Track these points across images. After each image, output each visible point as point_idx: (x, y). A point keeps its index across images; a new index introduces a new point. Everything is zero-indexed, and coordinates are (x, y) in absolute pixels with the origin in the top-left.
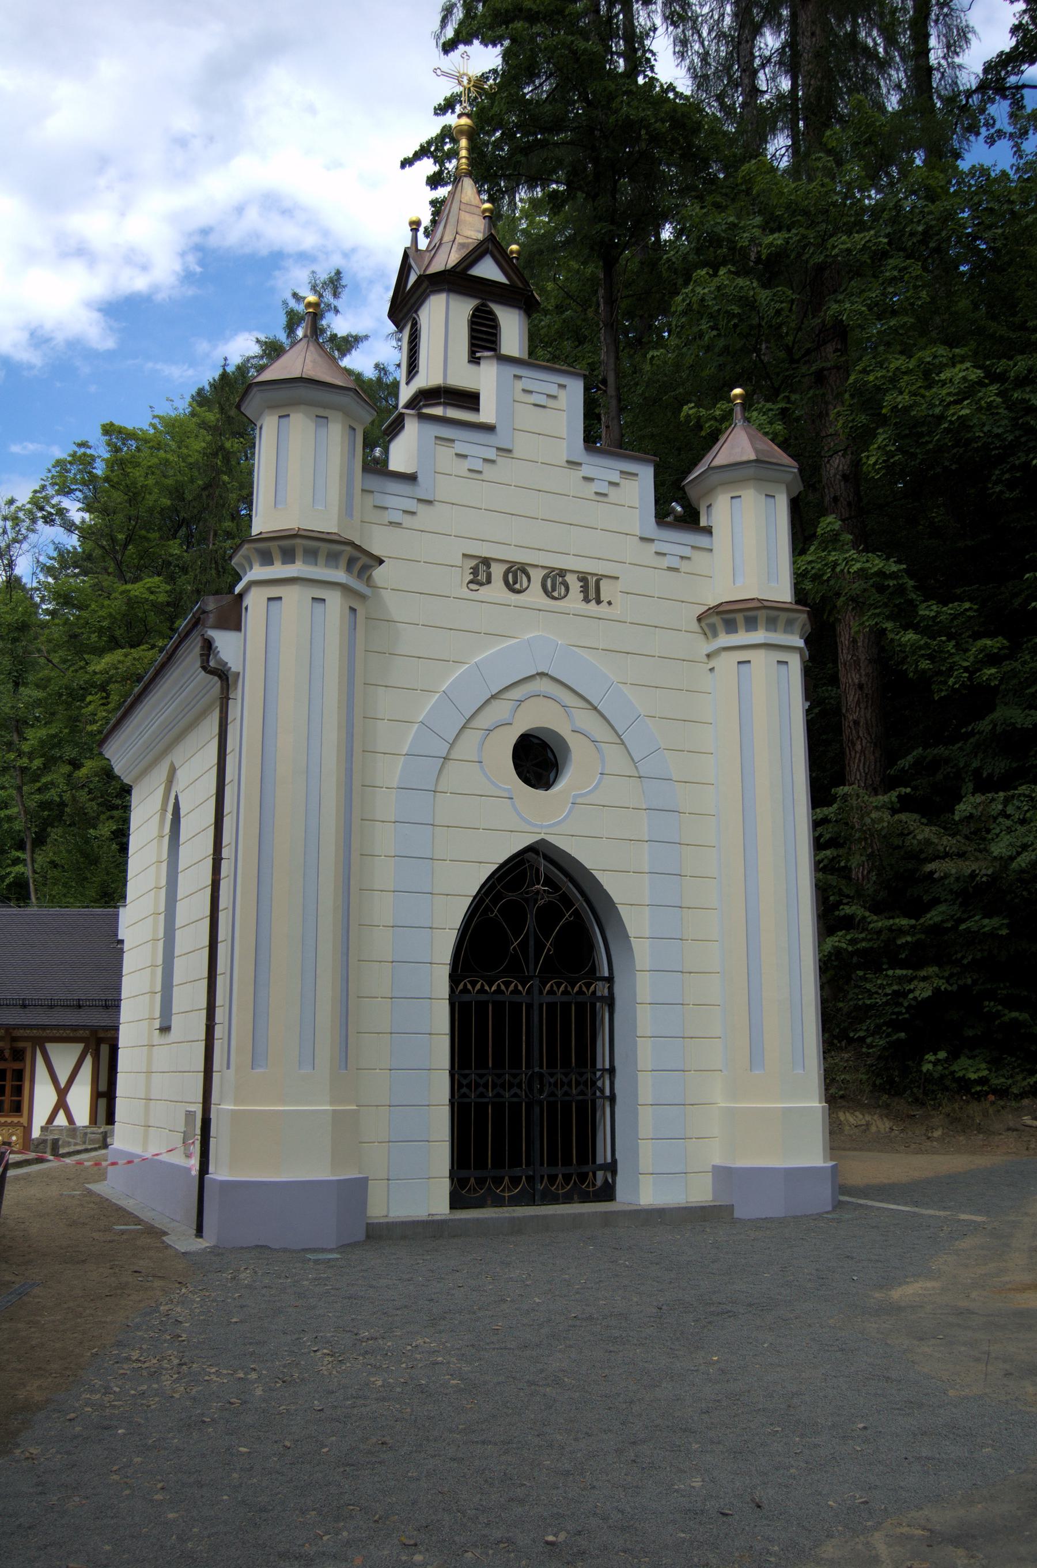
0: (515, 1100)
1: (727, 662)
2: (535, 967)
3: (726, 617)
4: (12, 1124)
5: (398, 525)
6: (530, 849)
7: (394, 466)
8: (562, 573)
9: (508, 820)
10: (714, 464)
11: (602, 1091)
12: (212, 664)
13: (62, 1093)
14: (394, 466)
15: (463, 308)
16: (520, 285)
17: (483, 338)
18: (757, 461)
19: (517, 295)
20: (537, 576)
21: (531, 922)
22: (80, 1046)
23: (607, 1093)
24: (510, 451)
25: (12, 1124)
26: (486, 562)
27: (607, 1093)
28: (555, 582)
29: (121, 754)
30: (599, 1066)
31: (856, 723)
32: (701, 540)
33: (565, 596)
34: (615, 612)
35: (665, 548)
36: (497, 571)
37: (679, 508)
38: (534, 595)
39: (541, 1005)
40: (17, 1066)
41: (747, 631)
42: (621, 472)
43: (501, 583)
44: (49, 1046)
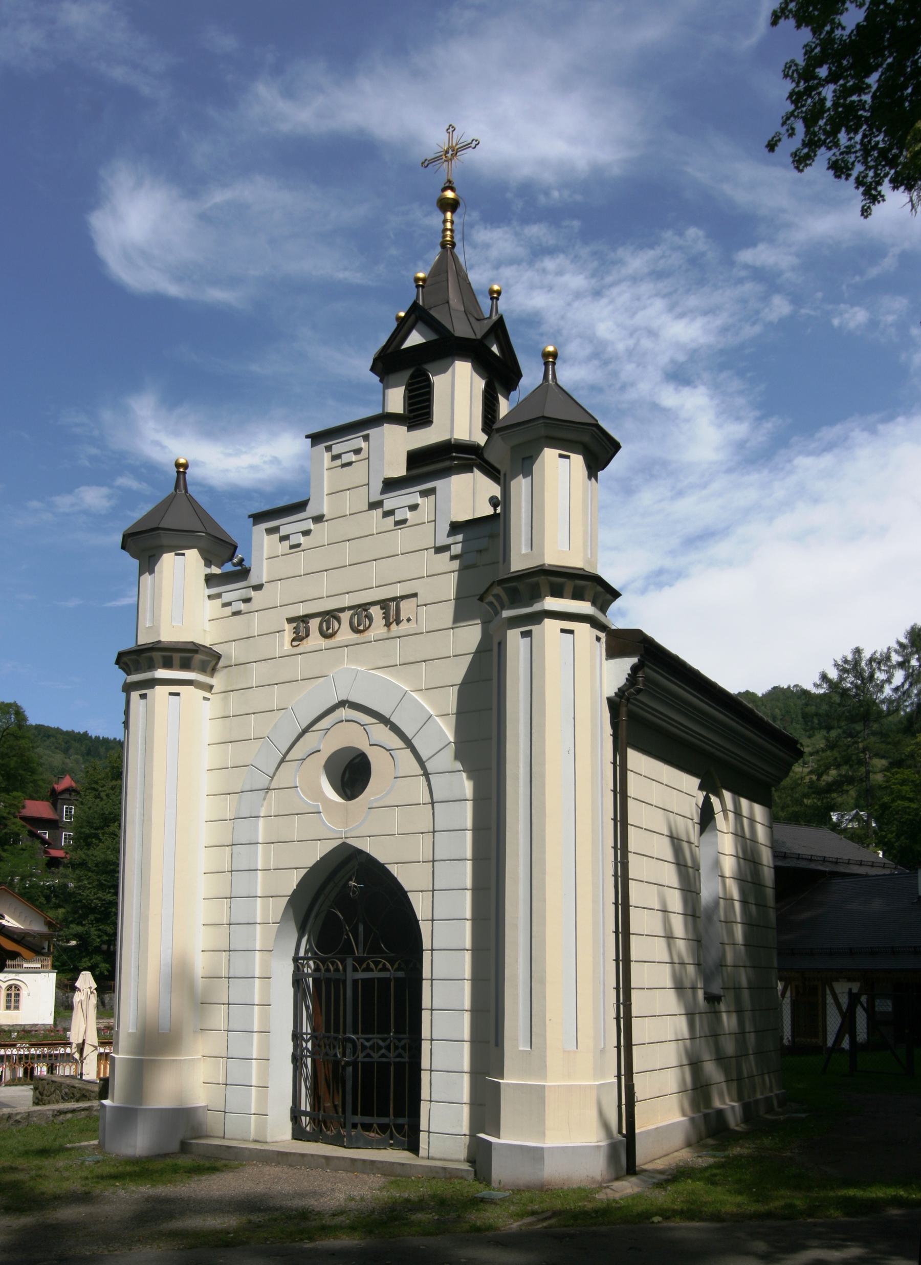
0: (384, 1060)
33: (370, 625)
38: (345, 634)
39: (355, 982)
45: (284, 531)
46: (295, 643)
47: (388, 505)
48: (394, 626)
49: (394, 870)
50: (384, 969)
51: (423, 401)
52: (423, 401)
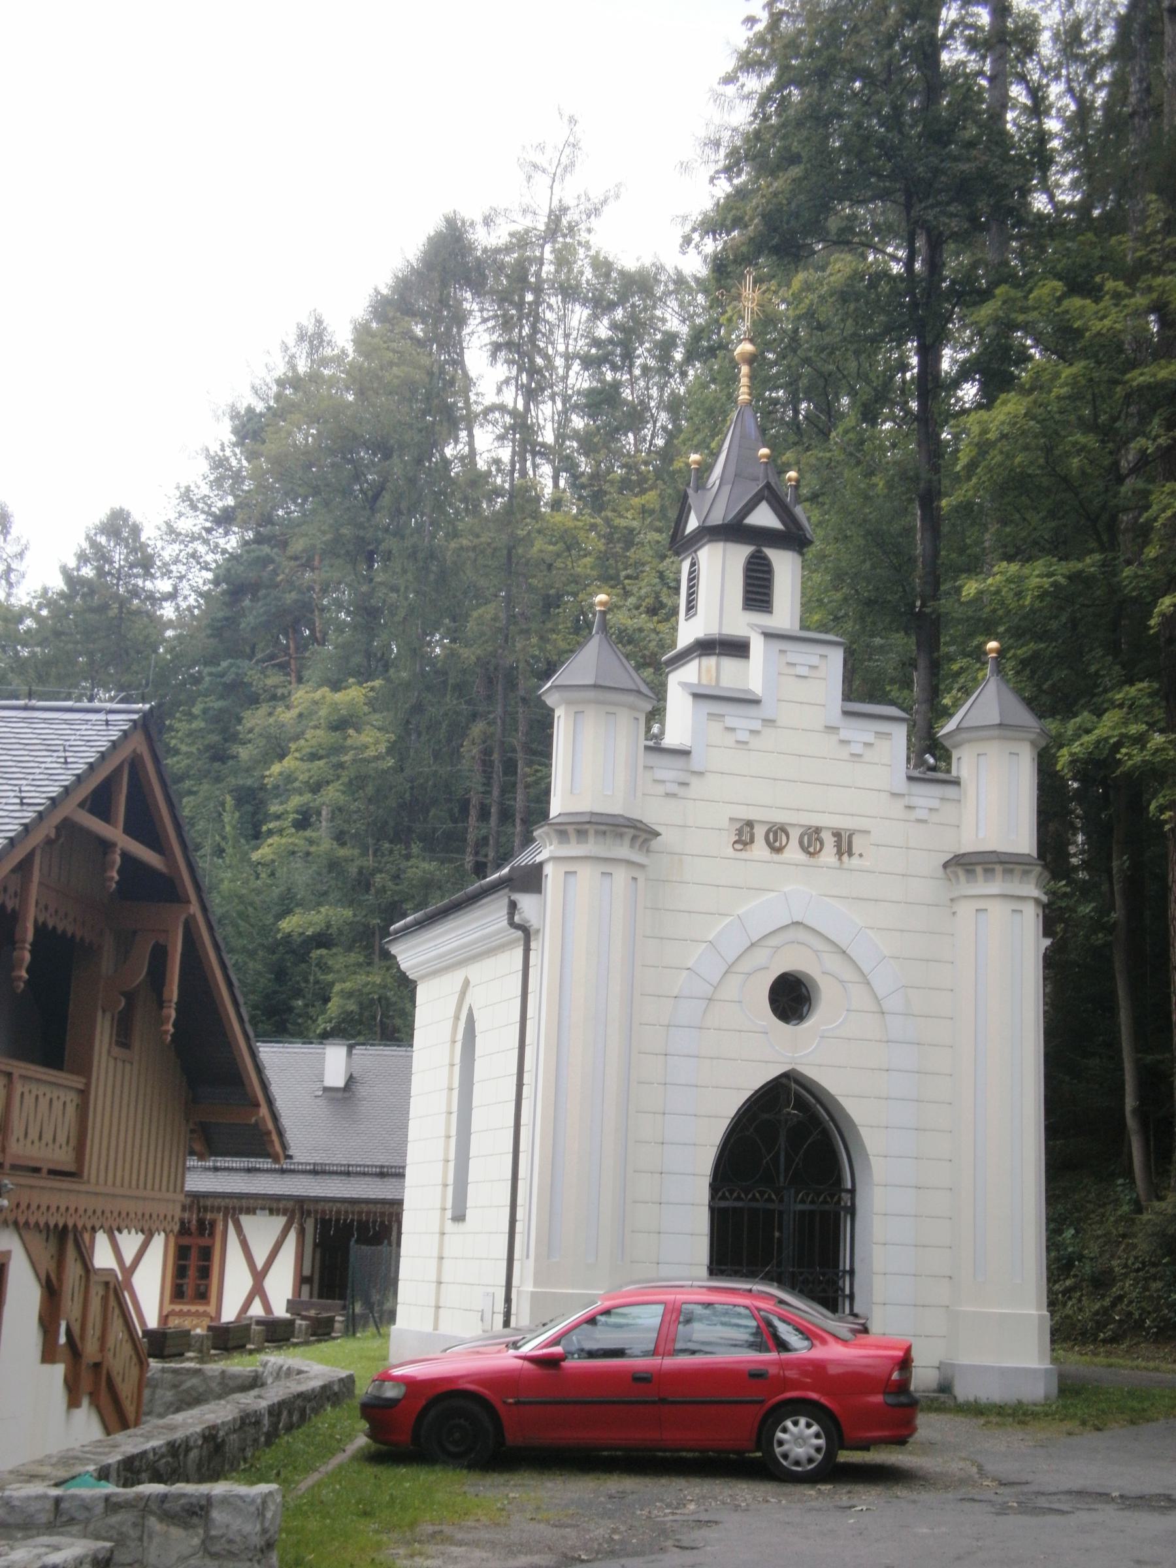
1: (966, 910)
2: (784, 1182)
3: (965, 864)
4: (197, 1314)
5: (674, 795)
6: (786, 1075)
7: (669, 741)
8: (818, 830)
9: (771, 1050)
10: (964, 725)
11: (843, 1290)
12: (517, 919)
13: (259, 1276)
14: (669, 741)
15: (740, 554)
16: (795, 530)
17: (758, 593)
18: (1000, 725)
19: (792, 538)
20: (795, 834)
21: (782, 1141)
22: (281, 1221)
23: (847, 1292)
24: (773, 721)
25: (197, 1314)
26: (750, 824)
27: (847, 1292)
28: (811, 840)
29: (410, 955)
30: (841, 1268)
32: (950, 791)
33: (821, 850)
34: (865, 863)
35: (916, 801)
36: (760, 832)
37: (931, 757)
38: (793, 852)
40: (204, 1242)
41: (986, 881)
42: (876, 733)
43: (763, 842)
44: (245, 1220)
45: (730, 722)
46: (736, 846)
47: (844, 734)
48: (845, 857)
49: (840, 1099)
50: (739, 1199)
51: (754, 564)
52: (754, 564)
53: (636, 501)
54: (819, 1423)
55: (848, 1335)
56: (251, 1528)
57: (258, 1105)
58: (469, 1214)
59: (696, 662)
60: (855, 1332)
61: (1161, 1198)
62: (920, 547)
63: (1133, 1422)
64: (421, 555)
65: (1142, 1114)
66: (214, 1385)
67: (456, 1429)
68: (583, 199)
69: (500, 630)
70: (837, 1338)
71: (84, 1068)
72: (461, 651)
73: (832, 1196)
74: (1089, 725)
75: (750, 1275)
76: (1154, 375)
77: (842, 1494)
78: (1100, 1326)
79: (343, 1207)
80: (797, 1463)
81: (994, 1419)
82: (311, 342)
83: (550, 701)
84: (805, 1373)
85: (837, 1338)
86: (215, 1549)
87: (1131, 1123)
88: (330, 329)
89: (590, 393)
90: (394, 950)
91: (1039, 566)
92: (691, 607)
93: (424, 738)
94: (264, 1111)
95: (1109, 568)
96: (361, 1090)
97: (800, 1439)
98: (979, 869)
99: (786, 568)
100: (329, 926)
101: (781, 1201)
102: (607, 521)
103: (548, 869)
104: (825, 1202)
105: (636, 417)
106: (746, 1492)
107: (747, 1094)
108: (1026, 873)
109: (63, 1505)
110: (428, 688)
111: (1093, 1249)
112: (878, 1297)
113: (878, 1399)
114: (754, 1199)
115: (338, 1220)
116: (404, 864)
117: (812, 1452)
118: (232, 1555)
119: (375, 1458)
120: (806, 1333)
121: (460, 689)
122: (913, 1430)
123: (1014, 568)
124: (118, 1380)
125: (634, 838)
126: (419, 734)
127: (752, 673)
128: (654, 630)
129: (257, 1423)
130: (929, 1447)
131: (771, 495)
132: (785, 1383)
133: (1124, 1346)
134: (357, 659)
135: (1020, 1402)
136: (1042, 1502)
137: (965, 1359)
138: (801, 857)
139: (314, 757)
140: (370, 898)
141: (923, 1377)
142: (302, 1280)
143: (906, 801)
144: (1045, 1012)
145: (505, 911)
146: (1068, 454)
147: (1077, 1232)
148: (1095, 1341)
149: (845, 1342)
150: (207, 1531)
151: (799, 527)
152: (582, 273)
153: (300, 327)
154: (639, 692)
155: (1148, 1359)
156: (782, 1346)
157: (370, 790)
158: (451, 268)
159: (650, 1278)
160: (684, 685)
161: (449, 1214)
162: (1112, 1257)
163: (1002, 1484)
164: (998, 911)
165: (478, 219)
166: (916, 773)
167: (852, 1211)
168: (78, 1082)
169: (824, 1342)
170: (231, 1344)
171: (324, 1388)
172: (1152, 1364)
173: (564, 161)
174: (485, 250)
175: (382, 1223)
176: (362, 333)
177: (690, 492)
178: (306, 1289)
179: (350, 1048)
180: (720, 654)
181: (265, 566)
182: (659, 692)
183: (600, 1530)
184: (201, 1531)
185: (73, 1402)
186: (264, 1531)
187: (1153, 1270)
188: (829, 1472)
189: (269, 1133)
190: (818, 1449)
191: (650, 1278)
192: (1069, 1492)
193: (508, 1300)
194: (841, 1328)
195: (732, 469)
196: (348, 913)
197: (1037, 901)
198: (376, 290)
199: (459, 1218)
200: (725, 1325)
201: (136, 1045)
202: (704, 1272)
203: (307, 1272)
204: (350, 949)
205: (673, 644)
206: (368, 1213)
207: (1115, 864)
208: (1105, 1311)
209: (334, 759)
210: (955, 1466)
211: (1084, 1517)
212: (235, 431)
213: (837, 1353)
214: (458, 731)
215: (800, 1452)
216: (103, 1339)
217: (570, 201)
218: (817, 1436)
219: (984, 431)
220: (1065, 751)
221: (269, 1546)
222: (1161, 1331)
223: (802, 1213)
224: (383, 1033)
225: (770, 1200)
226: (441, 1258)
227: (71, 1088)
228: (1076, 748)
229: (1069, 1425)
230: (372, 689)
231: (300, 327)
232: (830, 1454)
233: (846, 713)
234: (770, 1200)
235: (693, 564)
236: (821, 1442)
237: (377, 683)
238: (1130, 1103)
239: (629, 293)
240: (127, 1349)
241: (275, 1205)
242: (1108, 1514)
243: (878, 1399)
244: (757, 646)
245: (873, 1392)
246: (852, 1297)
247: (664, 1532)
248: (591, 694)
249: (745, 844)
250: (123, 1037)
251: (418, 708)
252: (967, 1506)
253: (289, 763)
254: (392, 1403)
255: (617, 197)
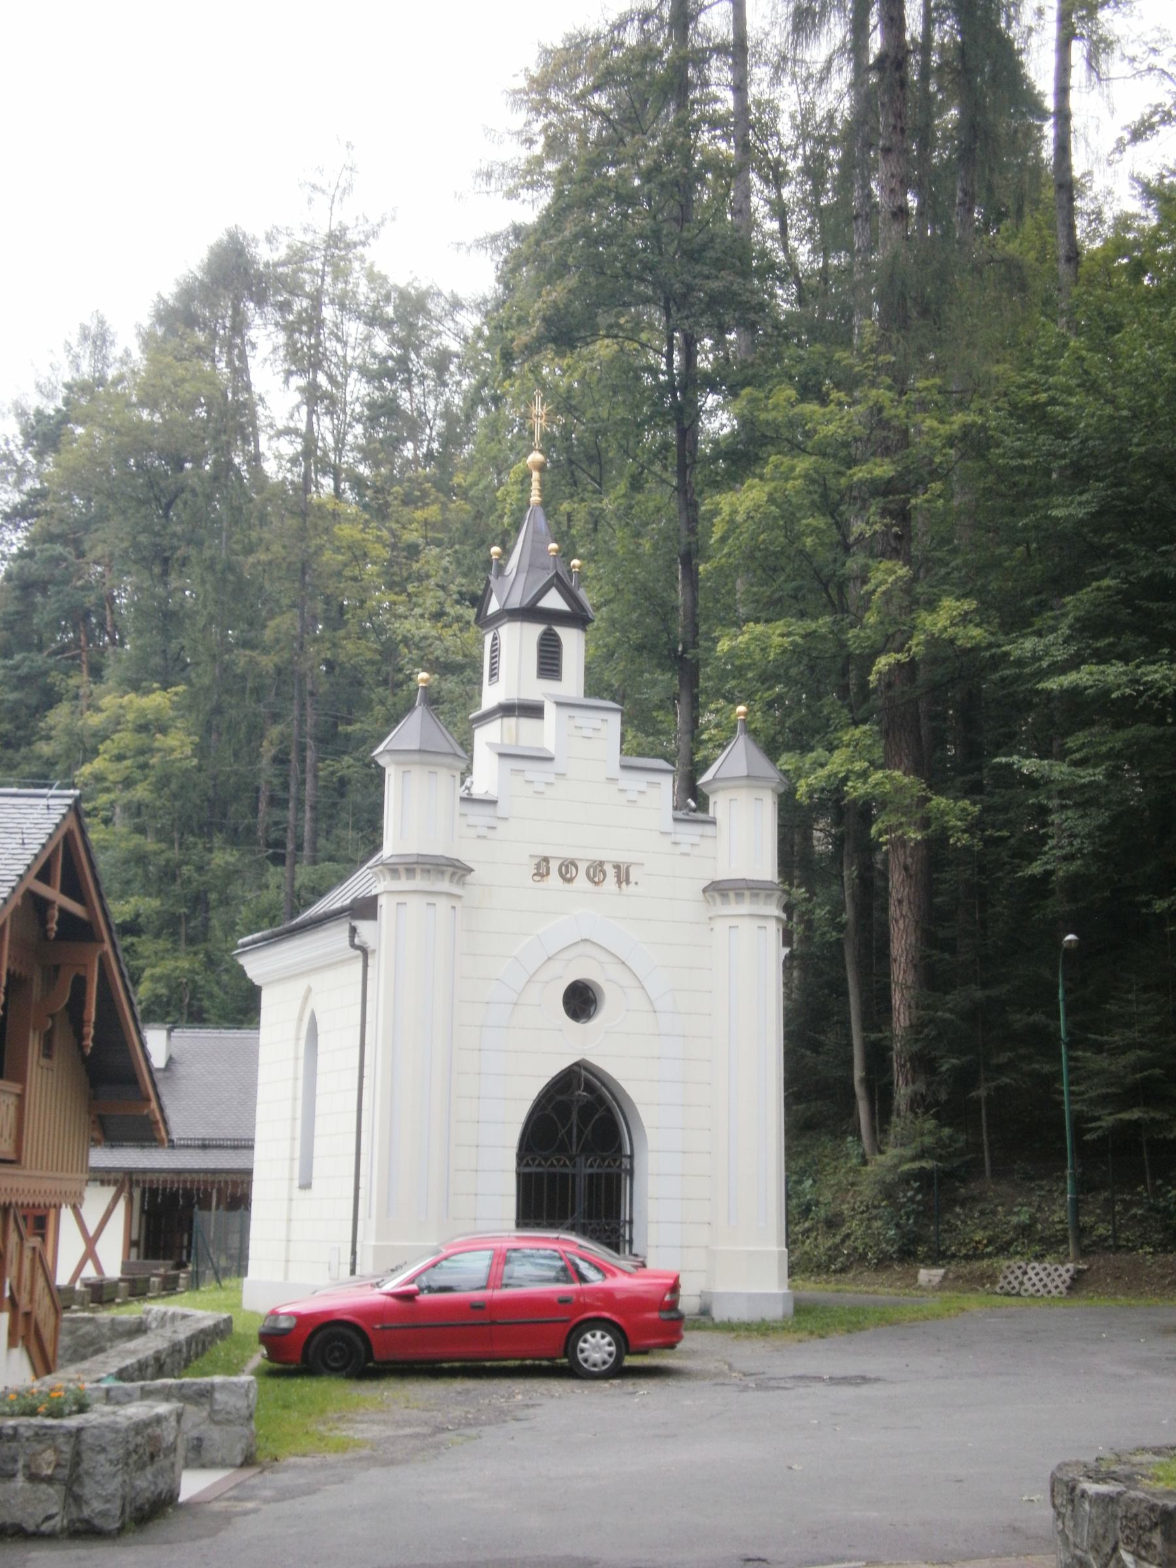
1: (721, 926)
2: (576, 1152)
3: (720, 890)
5: (484, 837)
6: (577, 1064)
7: (478, 791)
8: (601, 863)
9: (562, 1045)
12: (357, 941)
13: (91, 1242)
15: (535, 631)
17: (549, 662)
19: (577, 618)
20: (582, 867)
21: (575, 1117)
22: (110, 1191)
26: (546, 860)
28: (596, 872)
31: (900, 902)
32: (708, 830)
35: (678, 838)
36: (554, 866)
37: (693, 798)
38: (581, 882)
45: (529, 776)
47: (622, 784)
50: (540, 1165)
53: (419, 514)
54: (610, 1333)
55: (632, 1270)
56: (241, 1404)
57: (149, 1100)
58: (315, 1183)
59: (499, 722)
60: (636, 1267)
61: (881, 1152)
62: (680, 598)
63: (849, 1331)
64: (218, 567)
65: (868, 1082)
66: (105, 1330)
67: (326, 1349)
68: (361, 221)
69: (295, 638)
70: (624, 1272)
71: (20, 1077)
72: (259, 659)
73: (615, 1161)
74: (823, 760)
75: (552, 1226)
76: (870, 472)
77: (629, 1385)
78: (832, 1259)
79: (169, 1177)
80: (595, 1365)
81: (743, 1333)
82: (94, 342)
83: (382, 762)
84: (598, 1299)
85: (624, 1272)
86: (218, 1418)
87: (859, 1090)
88: (112, 330)
89: (371, 405)
90: (242, 961)
91: (779, 626)
92: (494, 674)
93: (224, 738)
94: (154, 1105)
95: (838, 633)
96: (181, 1070)
97: (596, 1347)
98: (732, 894)
99: (572, 642)
100: (138, 915)
101: (574, 1166)
102: (392, 532)
103: (382, 901)
104: (609, 1166)
105: (414, 426)
106: (557, 1386)
107: (548, 1080)
108: (769, 896)
109: (112, 1394)
110: (228, 691)
111: (827, 1196)
112: (652, 1240)
113: (654, 1315)
114: (552, 1165)
115: (164, 1189)
116: (208, 856)
117: (606, 1356)
118: (229, 1422)
119: (273, 1374)
120: (599, 1268)
121: (258, 692)
122: (680, 1338)
123: (760, 628)
124: (41, 1326)
125: (453, 874)
126: (220, 734)
127: (547, 733)
128: (439, 638)
129: (180, 1351)
130: (692, 1354)
131: (559, 583)
132: (586, 1307)
133: (850, 1275)
134: (156, 661)
135: (763, 1320)
136: (773, 1383)
137: (719, 1288)
138: (590, 885)
139: (120, 758)
140: (176, 888)
141: (688, 1303)
142: (131, 1244)
143: (673, 838)
144: (785, 1009)
145: (347, 934)
146: (803, 534)
147: (815, 1181)
148: (827, 1272)
149: (629, 1274)
150: (211, 1406)
151: (582, 607)
152: (357, 285)
153: (84, 329)
154: (455, 755)
155: (869, 1285)
156: (582, 1278)
157: (174, 786)
158: (235, 277)
159: (464, 1228)
160: (491, 745)
161: (296, 1183)
162: (843, 1202)
163: (745, 1375)
164: (748, 927)
165: (261, 237)
166: (680, 815)
167: (631, 1173)
168: (16, 1088)
169: (614, 1275)
170: (105, 1298)
171: (216, 1326)
172: (871, 1289)
173: (343, 184)
174: (267, 265)
175: (206, 1190)
176: (148, 341)
177: (492, 578)
178: (134, 1251)
179: (170, 1031)
180: (519, 716)
181: (58, 565)
182: (467, 745)
183: (457, 1412)
184: (207, 1407)
185: (12, 1343)
186: (249, 1406)
187: (875, 1212)
188: (617, 1371)
189: (156, 1122)
190: (610, 1355)
191: (464, 1228)
192: (794, 1377)
193: (354, 1253)
194: (626, 1264)
195: (526, 561)
196: (155, 903)
197: (778, 919)
198: (159, 295)
199: (306, 1185)
200: (538, 1264)
201: (55, 1057)
202: (513, 1224)
203: (135, 1236)
204: (157, 936)
205: (479, 705)
206: (192, 1182)
207: (846, 873)
208: (836, 1247)
209: (141, 759)
210: (712, 1366)
211: (801, 1390)
212: (25, 433)
213: (624, 1283)
214: (256, 732)
215: (597, 1356)
216: (32, 1292)
217: (350, 223)
218: (610, 1344)
219: (735, 512)
220: (802, 782)
221: (251, 1417)
222: (880, 1261)
223: (591, 1176)
224: (190, 1014)
225: (565, 1165)
226: (290, 1220)
227: (11, 1093)
228: (812, 780)
229: (799, 1335)
230: (176, 694)
231: (84, 329)
232: (619, 1358)
233: (624, 767)
234: (565, 1165)
235: (495, 639)
236: (613, 1349)
237: (181, 688)
238: (858, 1073)
239: (408, 314)
240: (47, 1301)
241: (106, 1177)
242: (819, 1388)
243: (654, 1315)
244: (550, 710)
245: (652, 1310)
246: (631, 1242)
247: (502, 1412)
248: (417, 757)
249: (542, 876)
250: (47, 1051)
251: (218, 710)
252: (718, 1388)
253: (98, 764)
254: (286, 1332)
255: (394, 219)
